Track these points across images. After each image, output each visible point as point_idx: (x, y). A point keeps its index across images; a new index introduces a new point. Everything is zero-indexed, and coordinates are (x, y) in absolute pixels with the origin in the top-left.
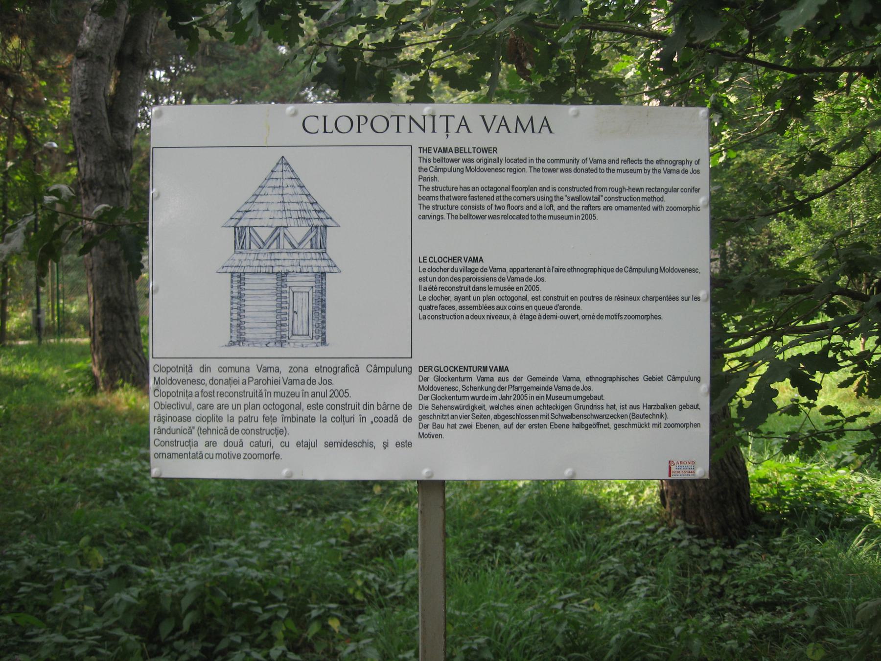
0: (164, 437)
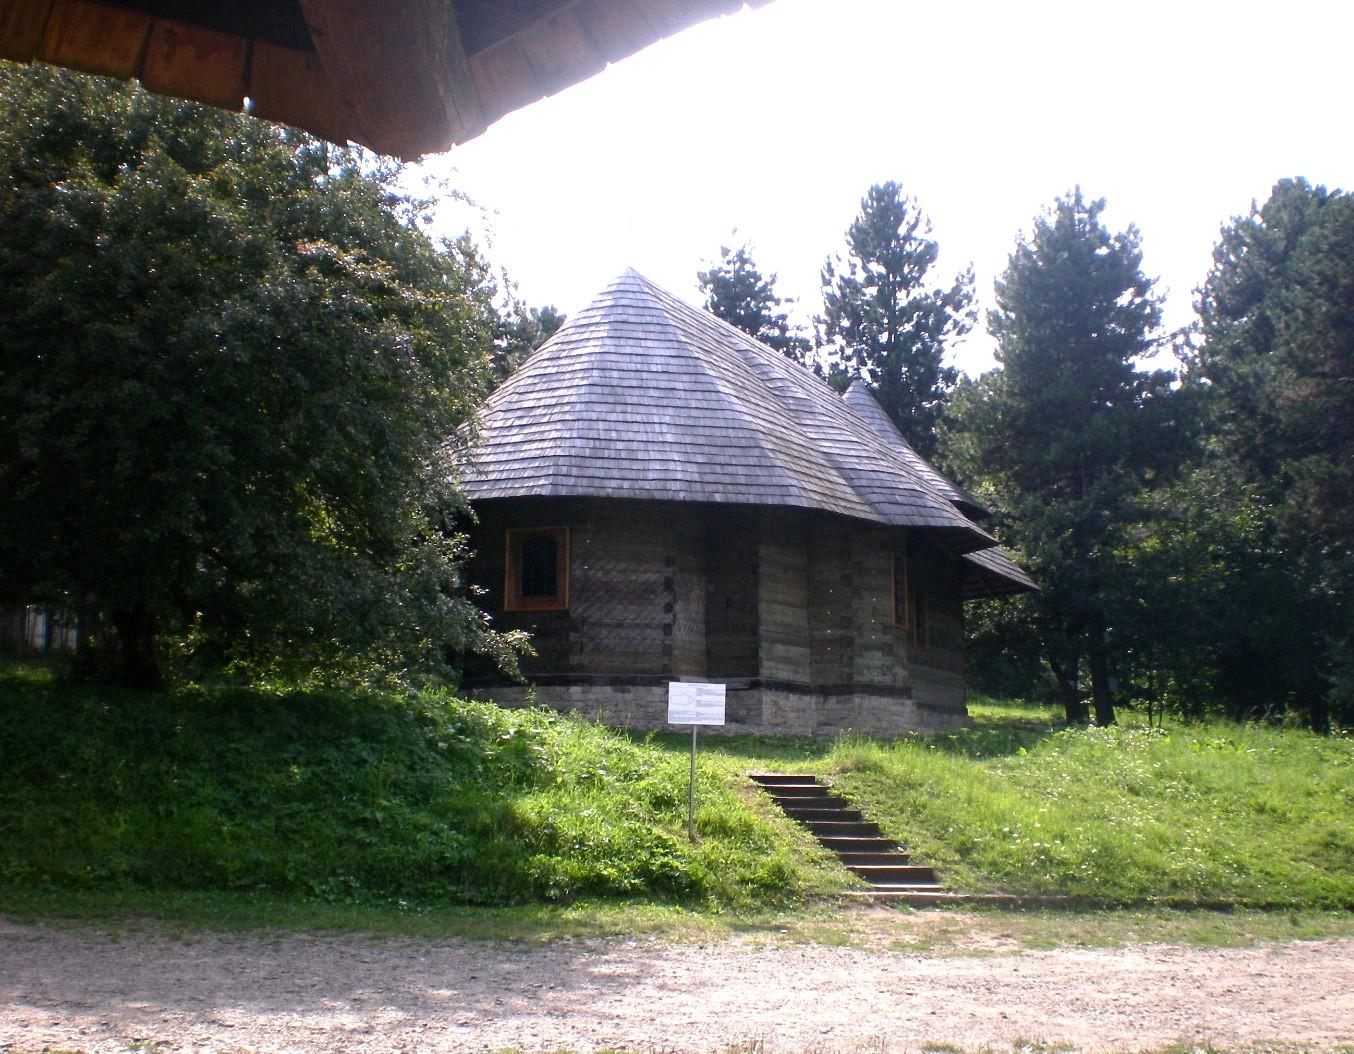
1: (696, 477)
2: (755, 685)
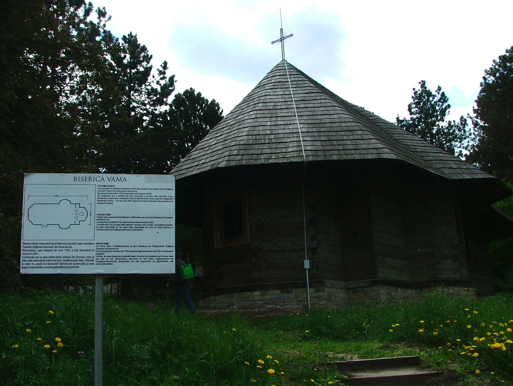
0: (24, 252)
1: (321, 148)
2: (375, 283)
